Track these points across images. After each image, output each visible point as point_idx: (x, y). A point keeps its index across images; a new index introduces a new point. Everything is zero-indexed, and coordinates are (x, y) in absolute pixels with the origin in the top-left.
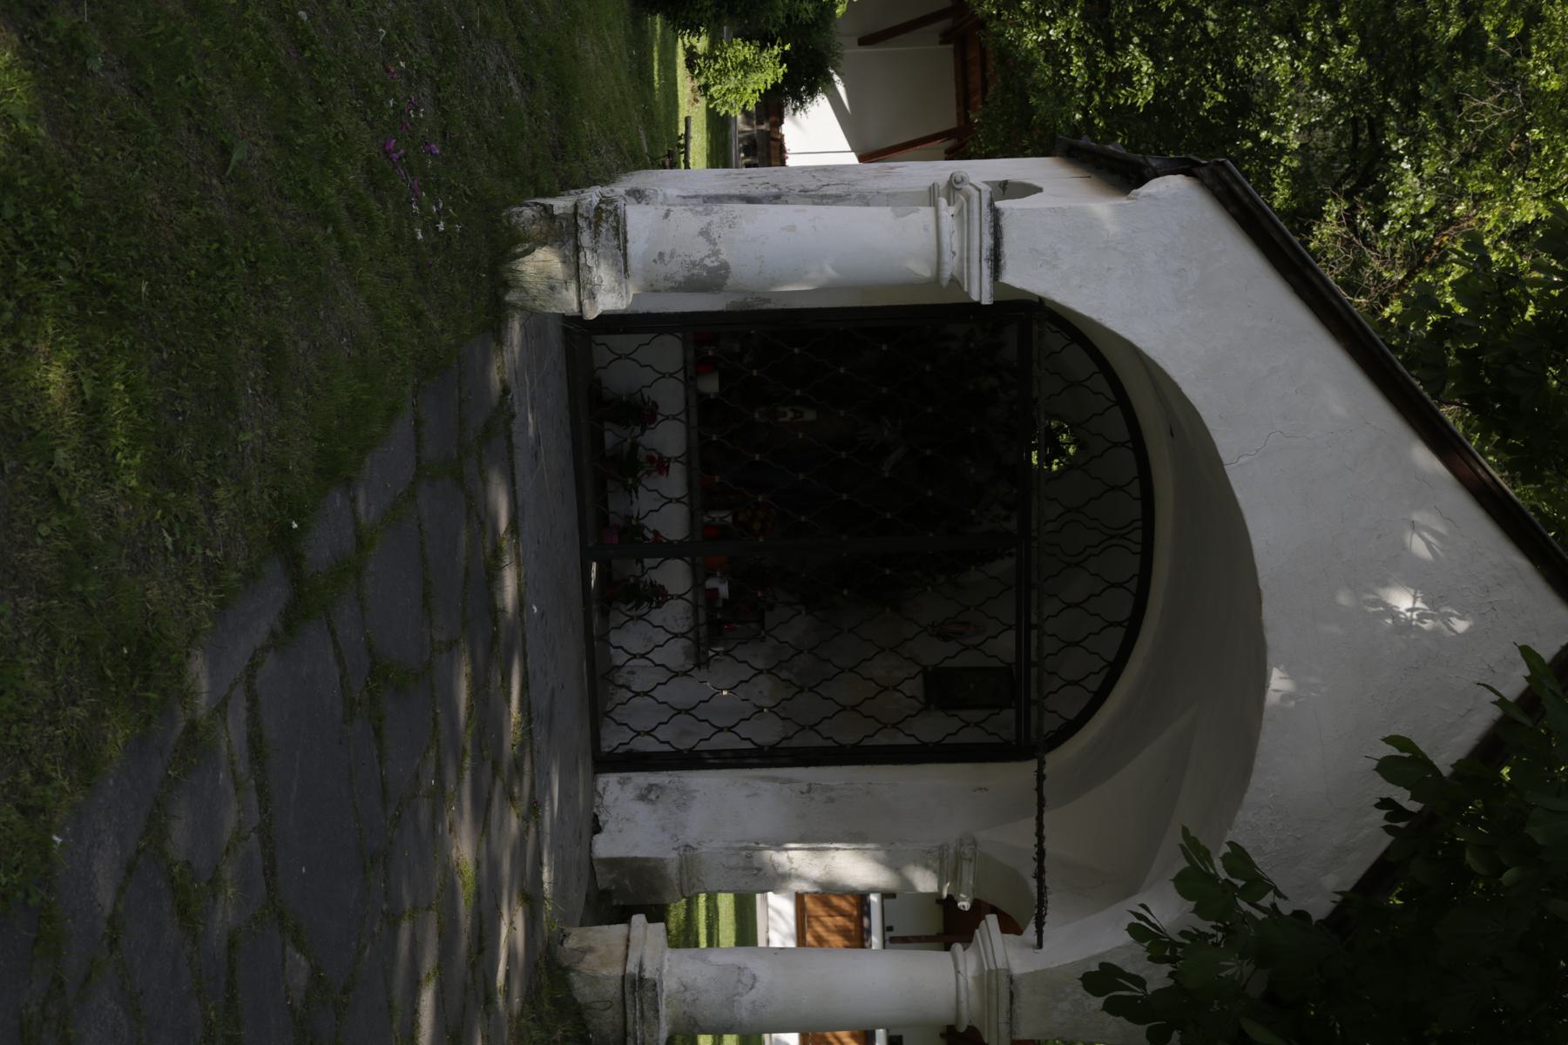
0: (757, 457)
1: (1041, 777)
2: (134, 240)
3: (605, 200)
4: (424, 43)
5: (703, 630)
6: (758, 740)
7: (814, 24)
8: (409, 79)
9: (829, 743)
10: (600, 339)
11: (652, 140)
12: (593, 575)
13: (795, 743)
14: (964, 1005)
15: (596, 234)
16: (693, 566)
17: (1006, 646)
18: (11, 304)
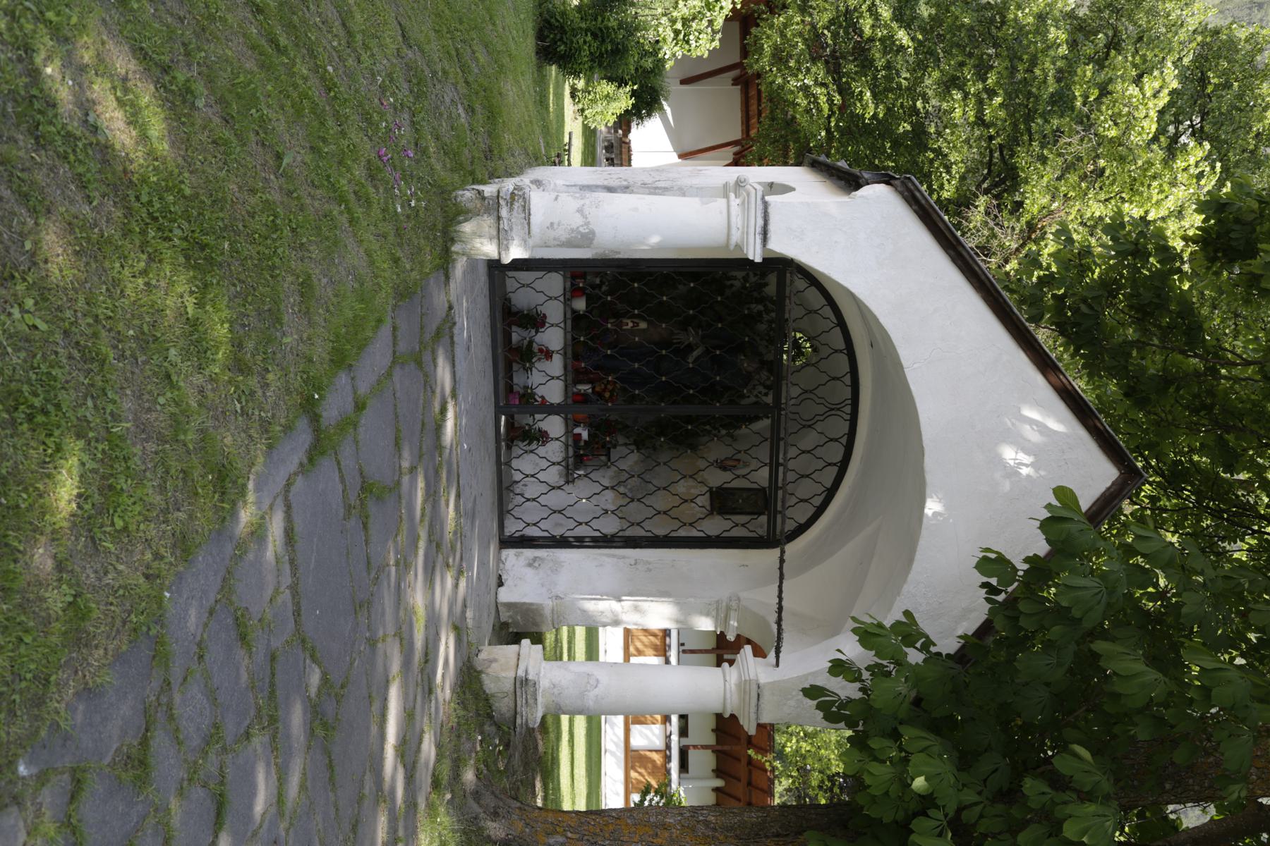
0: (609, 352)
1: (782, 561)
2: (221, 215)
3: (517, 188)
4: (406, 85)
5: (571, 460)
6: (604, 531)
7: (652, 71)
8: (395, 109)
9: (649, 534)
10: (510, 274)
11: (547, 145)
12: (503, 423)
13: (628, 533)
14: (728, 701)
15: (511, 210)
16: (566, 419)
17: (762, 477)
18: (144, 257)
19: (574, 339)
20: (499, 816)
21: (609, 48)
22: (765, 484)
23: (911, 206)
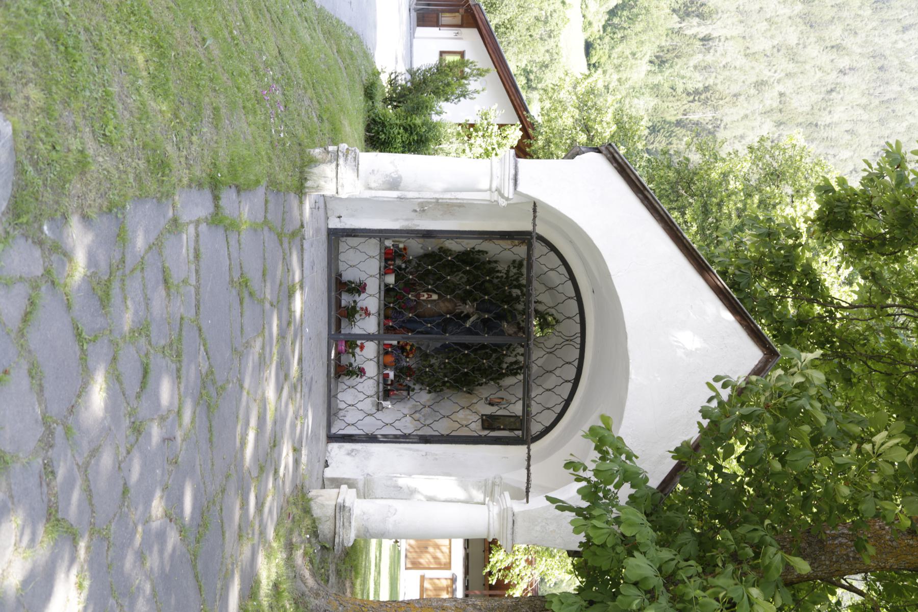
5: (381, 394)
14: (491, 529)
17: (517, 409)
19: (385, 305)
20: (319, 596)
21: (416, 138)
22: (520, 413)
23: (612, 164)
